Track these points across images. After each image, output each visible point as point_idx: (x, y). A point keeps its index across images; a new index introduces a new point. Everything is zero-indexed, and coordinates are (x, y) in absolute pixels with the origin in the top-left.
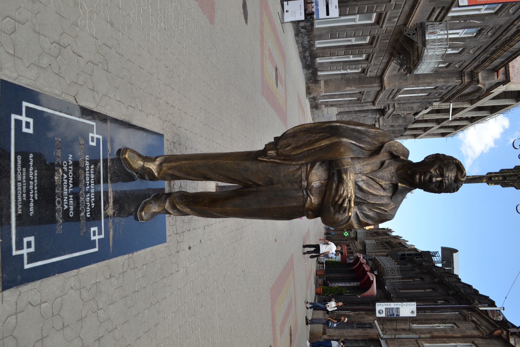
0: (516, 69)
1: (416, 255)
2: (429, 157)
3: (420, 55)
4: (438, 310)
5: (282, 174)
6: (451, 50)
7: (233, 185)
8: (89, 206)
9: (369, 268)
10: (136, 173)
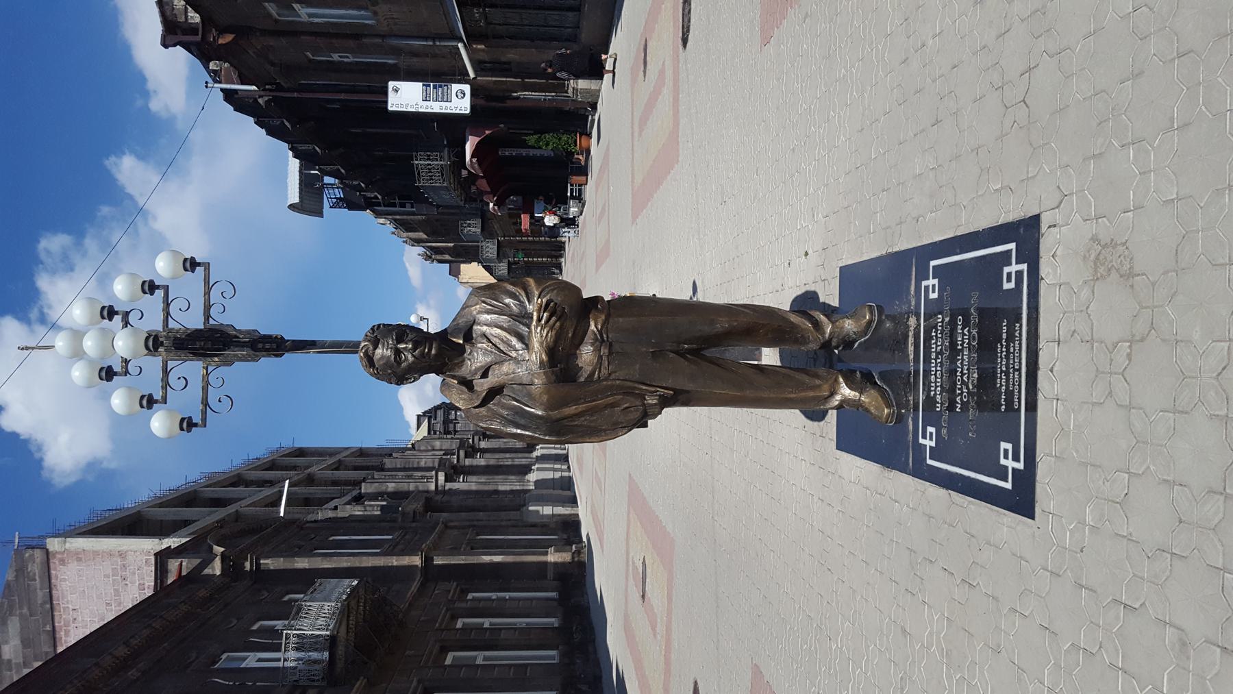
0: (135, 582)
2: (413, 379)
6: (275, 626)
8: (939, 332)
10: (877, 383)
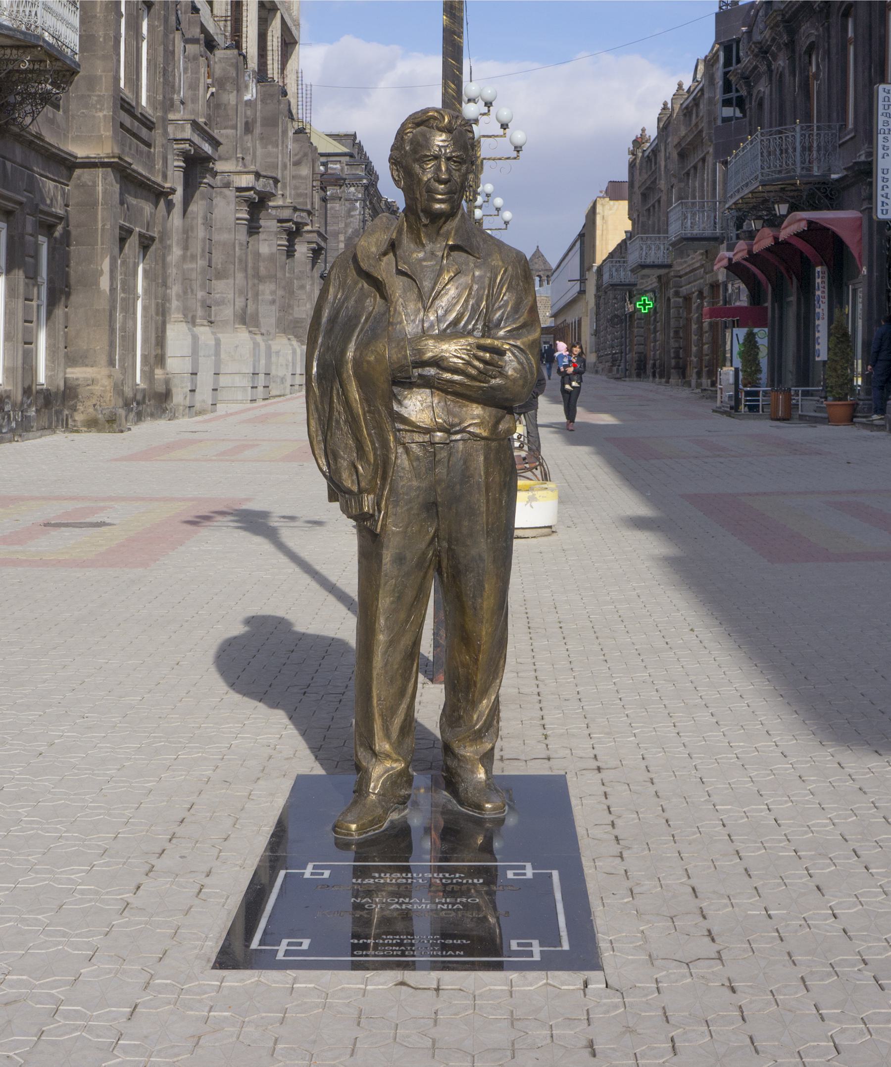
7: (433, 586)
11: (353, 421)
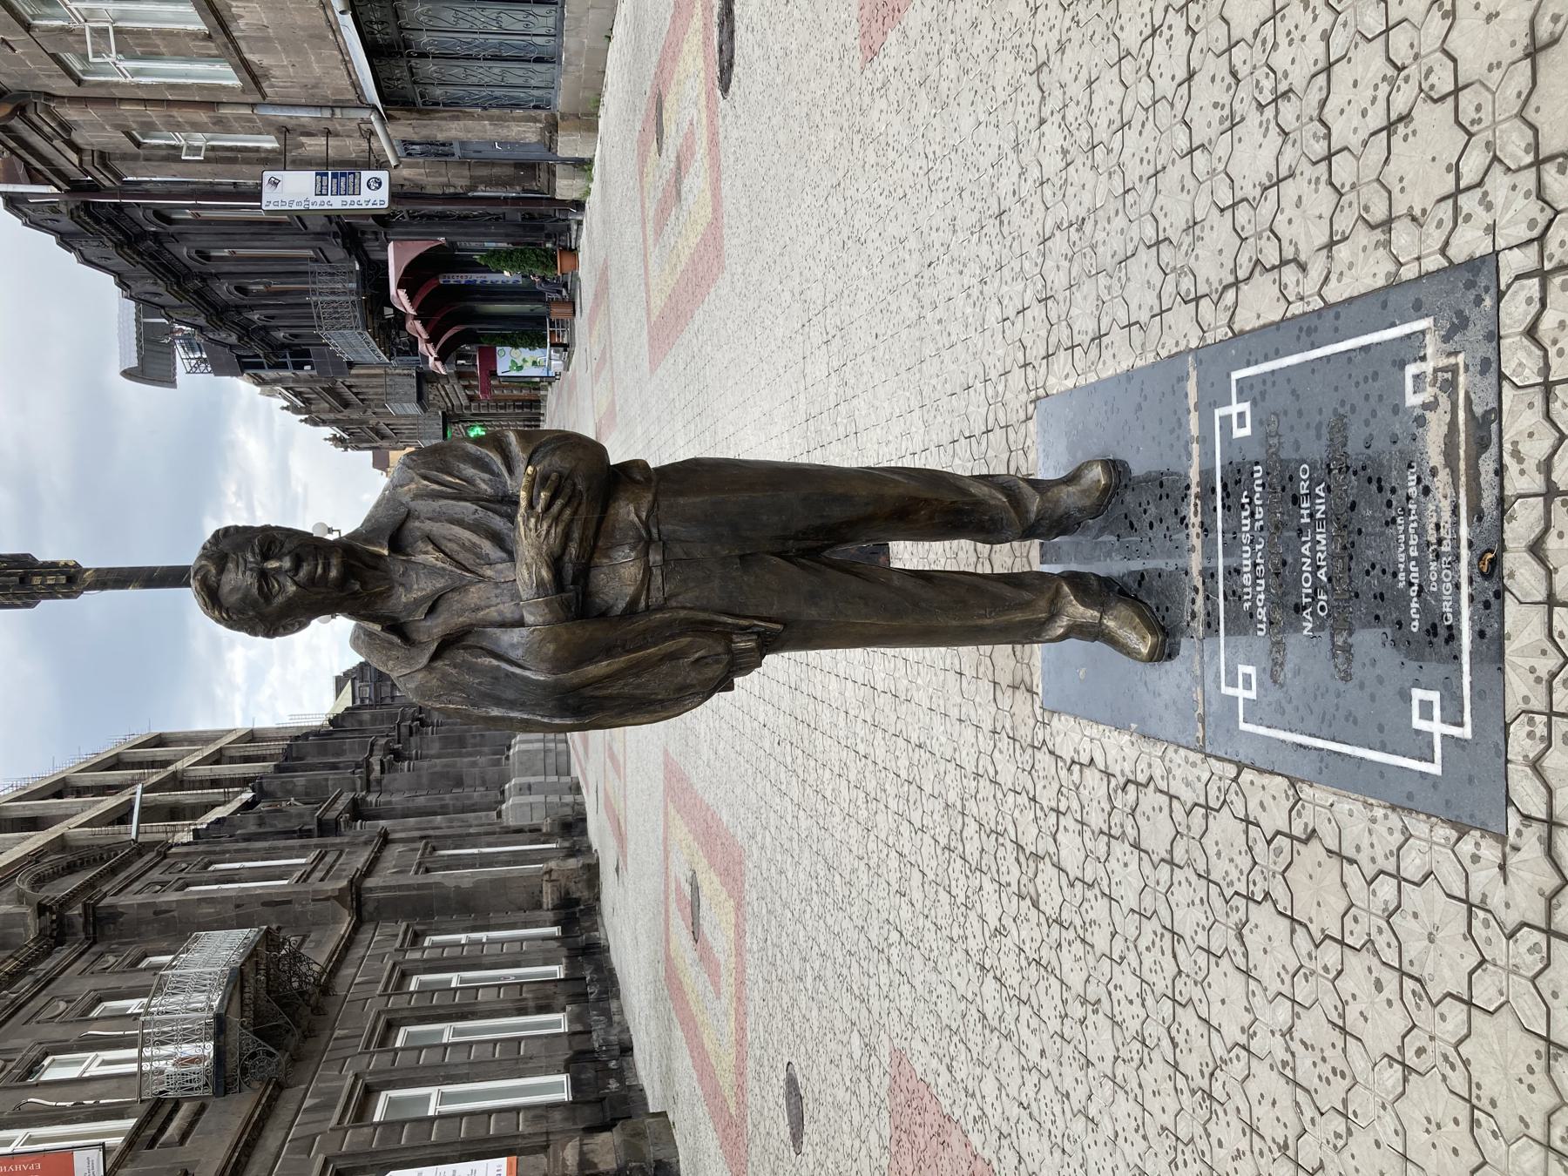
1: (260, 366)
3: (234, 987)
4: (193, 190)
5: (716, 583)
8: (1258, 495)
9: (408, 325)
11: (637, 668)
